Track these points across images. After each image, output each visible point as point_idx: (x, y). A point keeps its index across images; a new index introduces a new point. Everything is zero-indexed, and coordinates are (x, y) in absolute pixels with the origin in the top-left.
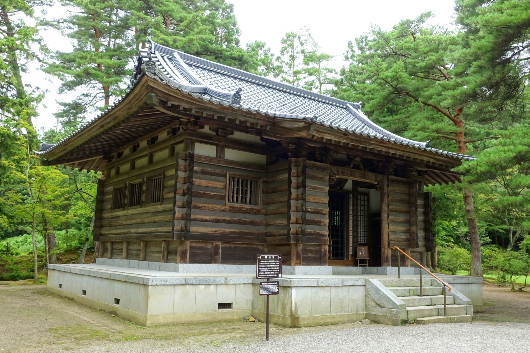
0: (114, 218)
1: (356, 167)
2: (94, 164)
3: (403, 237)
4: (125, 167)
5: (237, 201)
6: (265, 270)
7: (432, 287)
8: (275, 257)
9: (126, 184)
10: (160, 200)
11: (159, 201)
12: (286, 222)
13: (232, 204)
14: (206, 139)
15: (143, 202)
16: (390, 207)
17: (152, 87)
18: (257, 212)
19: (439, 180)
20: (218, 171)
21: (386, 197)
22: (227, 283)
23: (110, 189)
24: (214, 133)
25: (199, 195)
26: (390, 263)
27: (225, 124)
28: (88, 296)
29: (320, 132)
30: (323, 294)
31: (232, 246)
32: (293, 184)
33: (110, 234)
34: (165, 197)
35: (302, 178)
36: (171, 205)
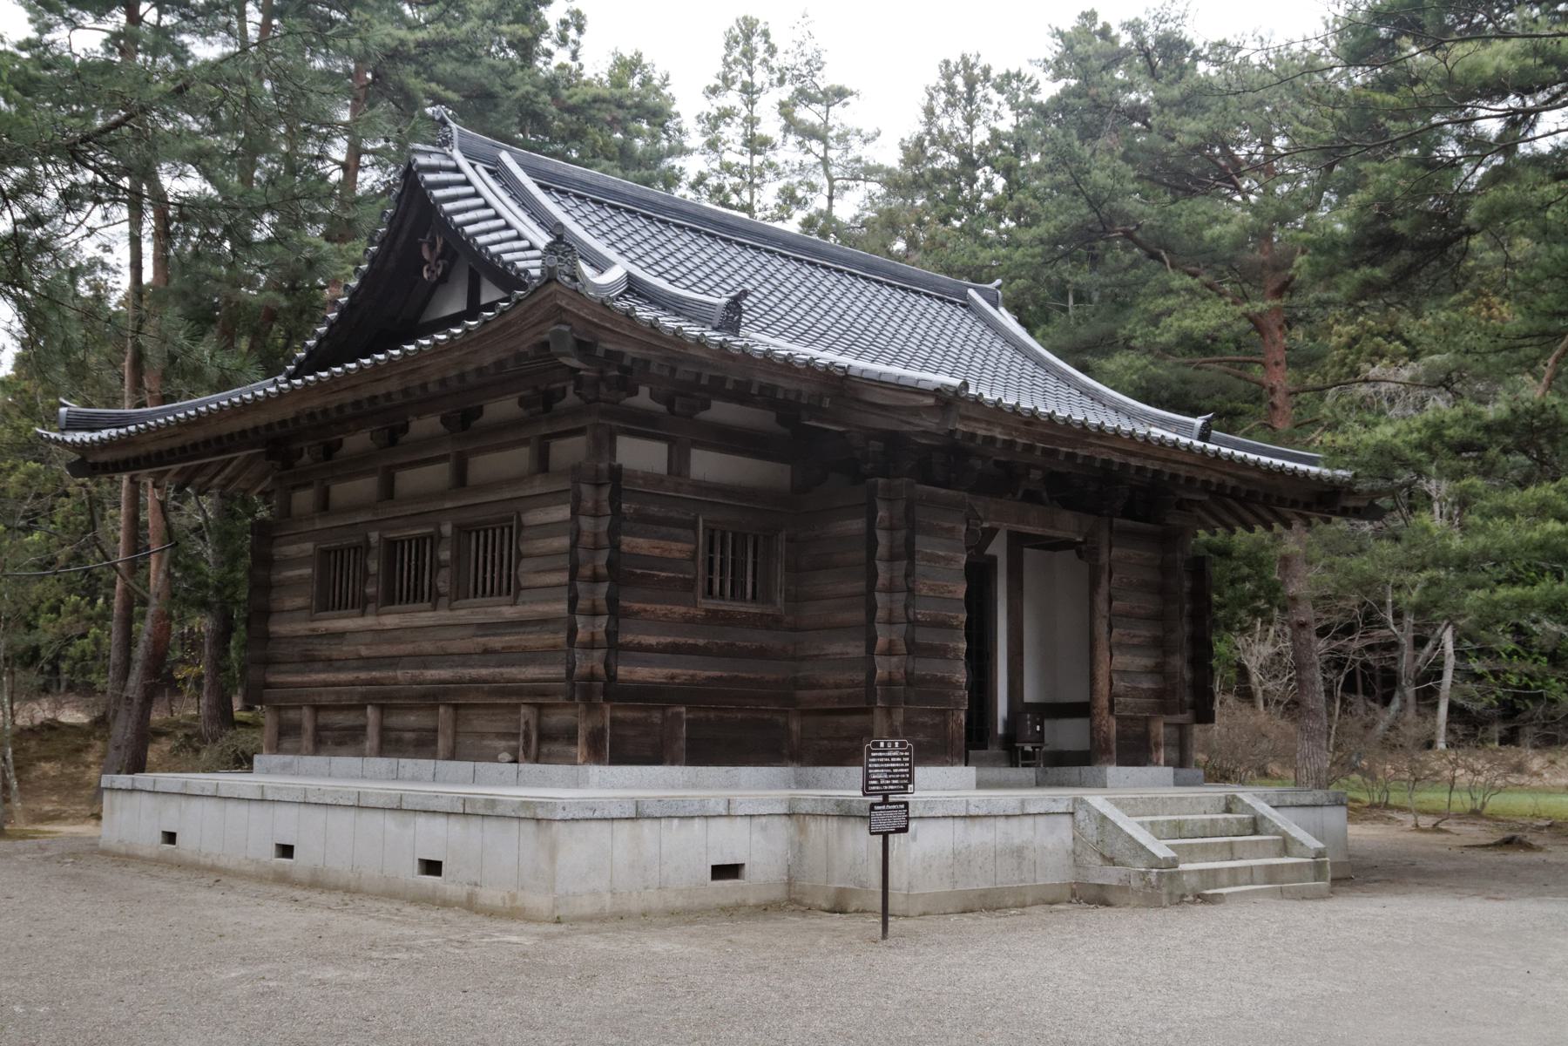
1: (1031, 497)
2: (227, 471)
3: (1145, 685)
7: (1229, 816)
12: (863, 650)
13: (712, 604)
14: (643, 426)
18: (770, 623)
21: (1105, 577)
24: (662, 408)
29: (969, 418)
30: (980, 835)
31: (712, 715)
33: (303, 685)
34: (524, 583)
35: (904, 532)
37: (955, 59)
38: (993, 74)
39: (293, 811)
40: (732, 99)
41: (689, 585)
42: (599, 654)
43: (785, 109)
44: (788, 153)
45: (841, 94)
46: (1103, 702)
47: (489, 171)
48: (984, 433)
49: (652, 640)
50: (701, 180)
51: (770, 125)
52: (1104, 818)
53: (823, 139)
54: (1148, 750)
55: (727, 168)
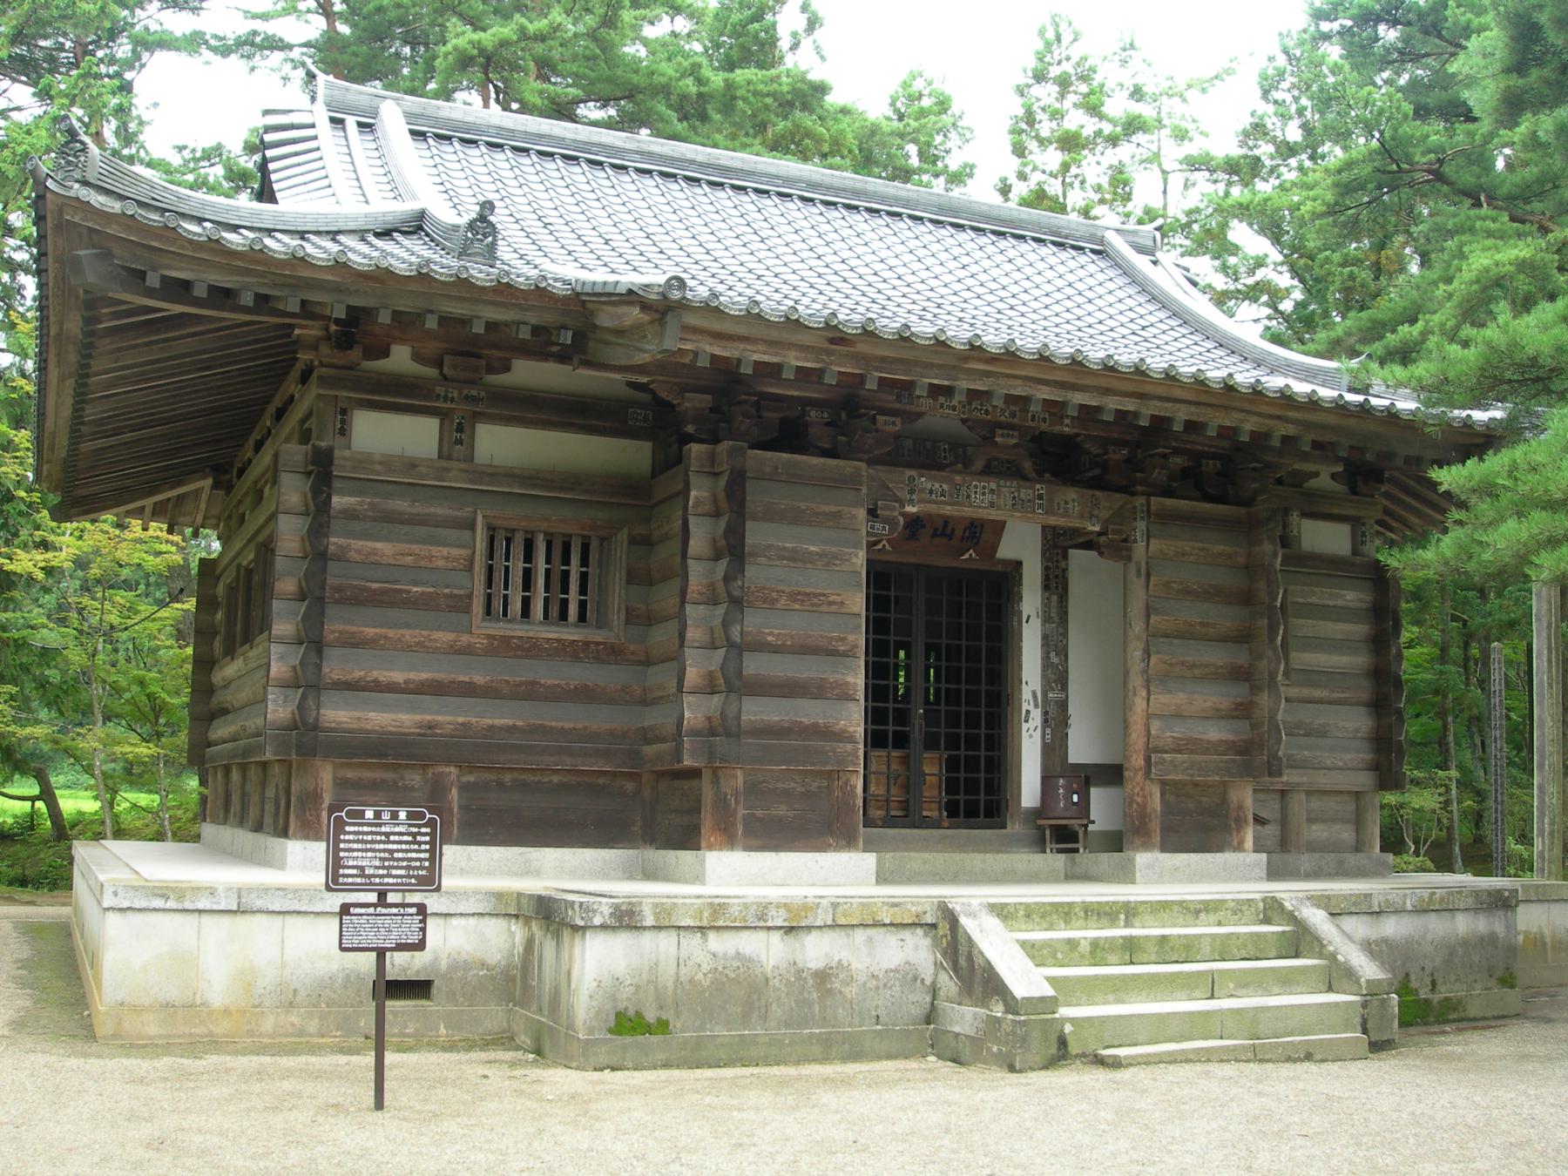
5: (526, 612)
6: (369, 862)
8: (410, 816)
13: (499, 629)
14: (397, 395)
16: (1153, 619)
18: (613, 654)
20: (441, 510)
24: (432, 372)
25: (358, 599)
26: (1157, 839)
46: (1138, 761)
49: (398, 677)
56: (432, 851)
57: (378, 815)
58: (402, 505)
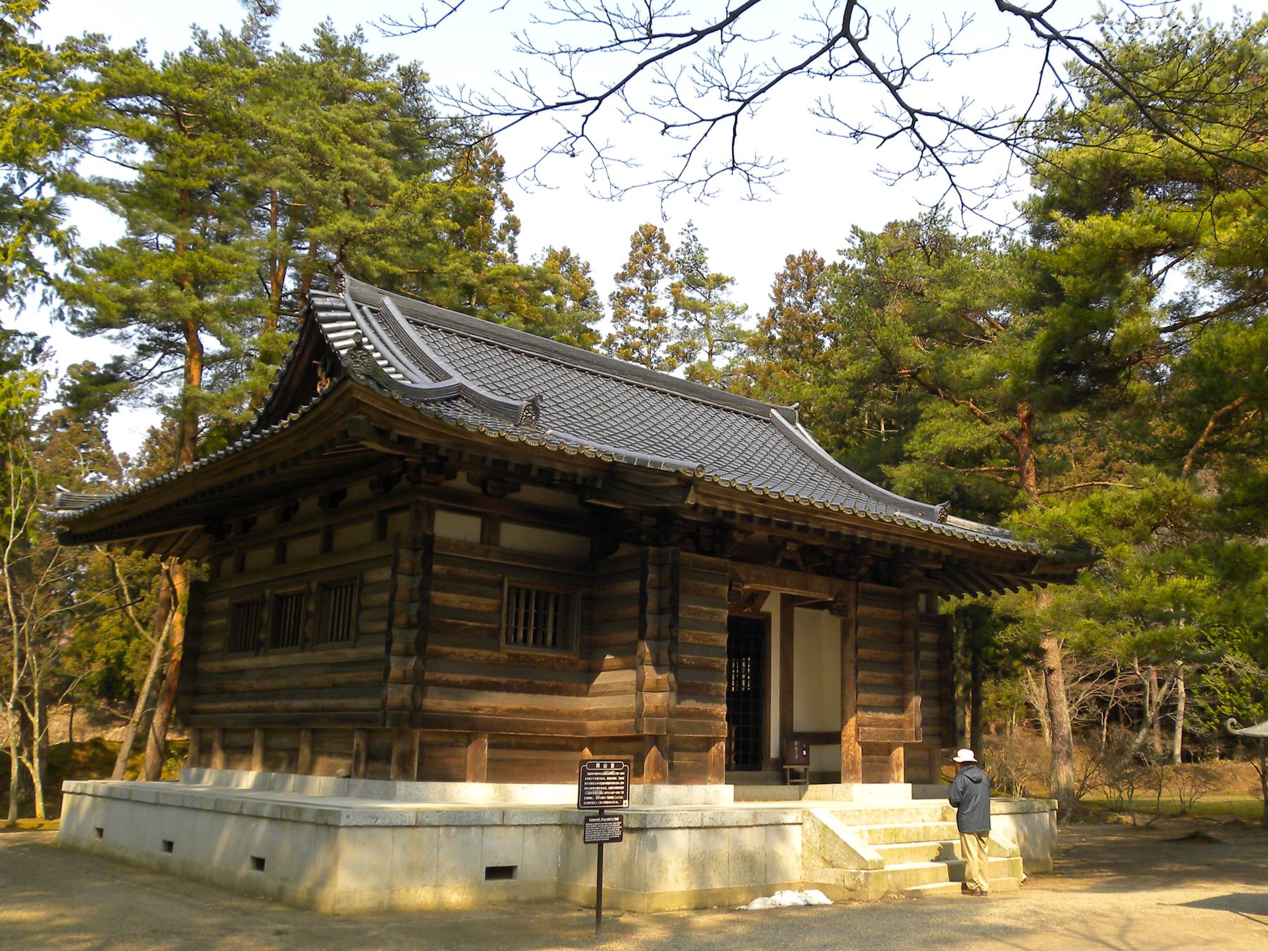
0: (230, 673)
1: (789, 565)
2: (180, 542)
4: (261, 556)
9: (263, 595)
10: (345, 633)
11: (348, 639)
13: (514, 650)
14: (459, 503)
15: (306, 640)
16: (860, 651)
17: (359, 402)
19: (983, 582)
21: (852, 629)
22: (506, 822)
23: (223, 603)
24: (477, 490)
27: (508, 476)
28: (178, 854)
32: (651, 604)
36: (380, 650)
37: (798, 254)
38: (826, 265)
39: (176, 814)
40: (637, 283)
41: (494, 634)
42: (408, 688)
43: (675, 290)
44: (674, 322)
45: (719, 281)
47: (373, 311)
48: (725, 508)
49: (459, 678)
50: (611, 339)
51: (663, 302)
52: (825, 827)
53: (704, 312)
54: (890, 769)
55: (633, 332)
56: (625, 785)
57: (602, 766)
58: (464, 571)
